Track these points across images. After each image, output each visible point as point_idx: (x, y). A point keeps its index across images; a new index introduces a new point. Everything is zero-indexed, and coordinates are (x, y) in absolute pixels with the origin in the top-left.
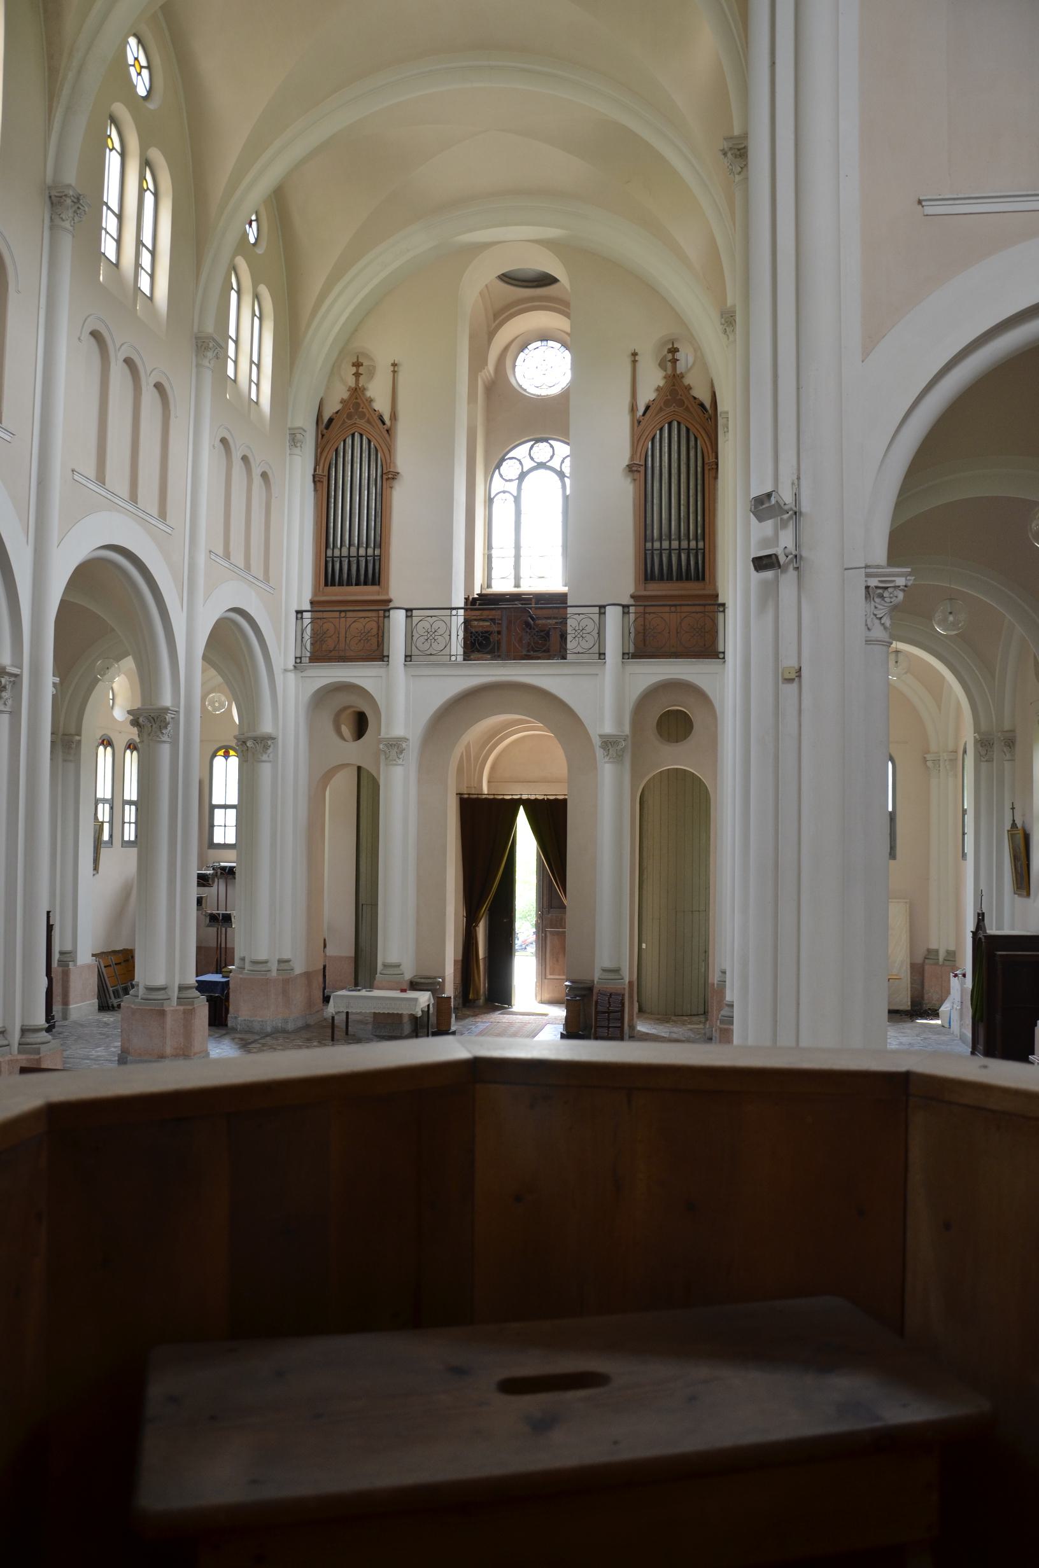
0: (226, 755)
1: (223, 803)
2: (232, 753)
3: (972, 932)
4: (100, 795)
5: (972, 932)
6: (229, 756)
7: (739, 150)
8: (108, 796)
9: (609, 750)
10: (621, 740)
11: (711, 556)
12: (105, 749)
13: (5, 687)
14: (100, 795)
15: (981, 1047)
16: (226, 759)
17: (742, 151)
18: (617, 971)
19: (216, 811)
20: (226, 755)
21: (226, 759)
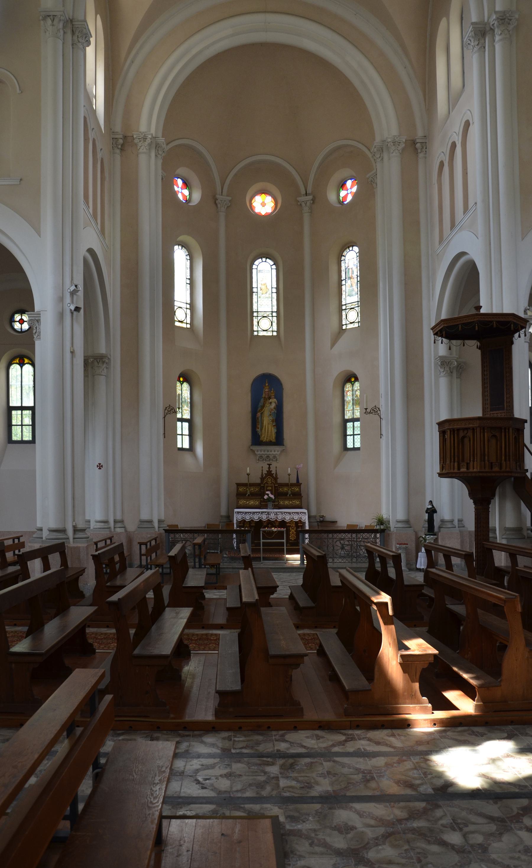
0: (22, 364)
1: (19, 405)
2: (26, 361)
3: (438, 473)
4: (15, 402)
5: (438, 473)
6: (24, 364)
7: (139, 139)
8: (29, 402)
9: (444, 367)
10: (454, 361)
11: (74, 267)
12: (182, 384)
13: (529, 306)
14: (15, 402)
15: (277, 556)
16: (22, 367)
17: (140, 139)
18: (63, 531)
19: (14, 412)
20: (22, 364)
21: (22, 367)
